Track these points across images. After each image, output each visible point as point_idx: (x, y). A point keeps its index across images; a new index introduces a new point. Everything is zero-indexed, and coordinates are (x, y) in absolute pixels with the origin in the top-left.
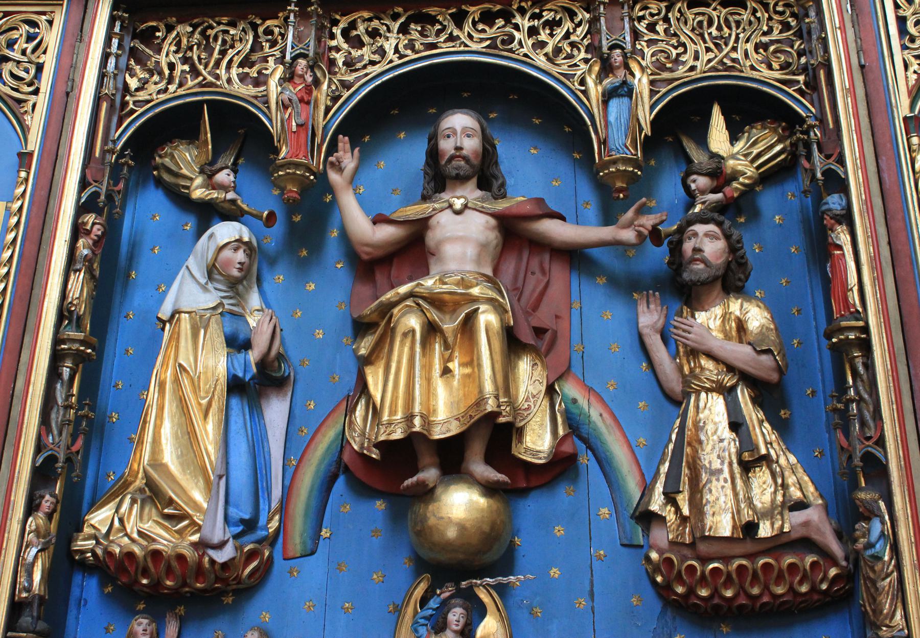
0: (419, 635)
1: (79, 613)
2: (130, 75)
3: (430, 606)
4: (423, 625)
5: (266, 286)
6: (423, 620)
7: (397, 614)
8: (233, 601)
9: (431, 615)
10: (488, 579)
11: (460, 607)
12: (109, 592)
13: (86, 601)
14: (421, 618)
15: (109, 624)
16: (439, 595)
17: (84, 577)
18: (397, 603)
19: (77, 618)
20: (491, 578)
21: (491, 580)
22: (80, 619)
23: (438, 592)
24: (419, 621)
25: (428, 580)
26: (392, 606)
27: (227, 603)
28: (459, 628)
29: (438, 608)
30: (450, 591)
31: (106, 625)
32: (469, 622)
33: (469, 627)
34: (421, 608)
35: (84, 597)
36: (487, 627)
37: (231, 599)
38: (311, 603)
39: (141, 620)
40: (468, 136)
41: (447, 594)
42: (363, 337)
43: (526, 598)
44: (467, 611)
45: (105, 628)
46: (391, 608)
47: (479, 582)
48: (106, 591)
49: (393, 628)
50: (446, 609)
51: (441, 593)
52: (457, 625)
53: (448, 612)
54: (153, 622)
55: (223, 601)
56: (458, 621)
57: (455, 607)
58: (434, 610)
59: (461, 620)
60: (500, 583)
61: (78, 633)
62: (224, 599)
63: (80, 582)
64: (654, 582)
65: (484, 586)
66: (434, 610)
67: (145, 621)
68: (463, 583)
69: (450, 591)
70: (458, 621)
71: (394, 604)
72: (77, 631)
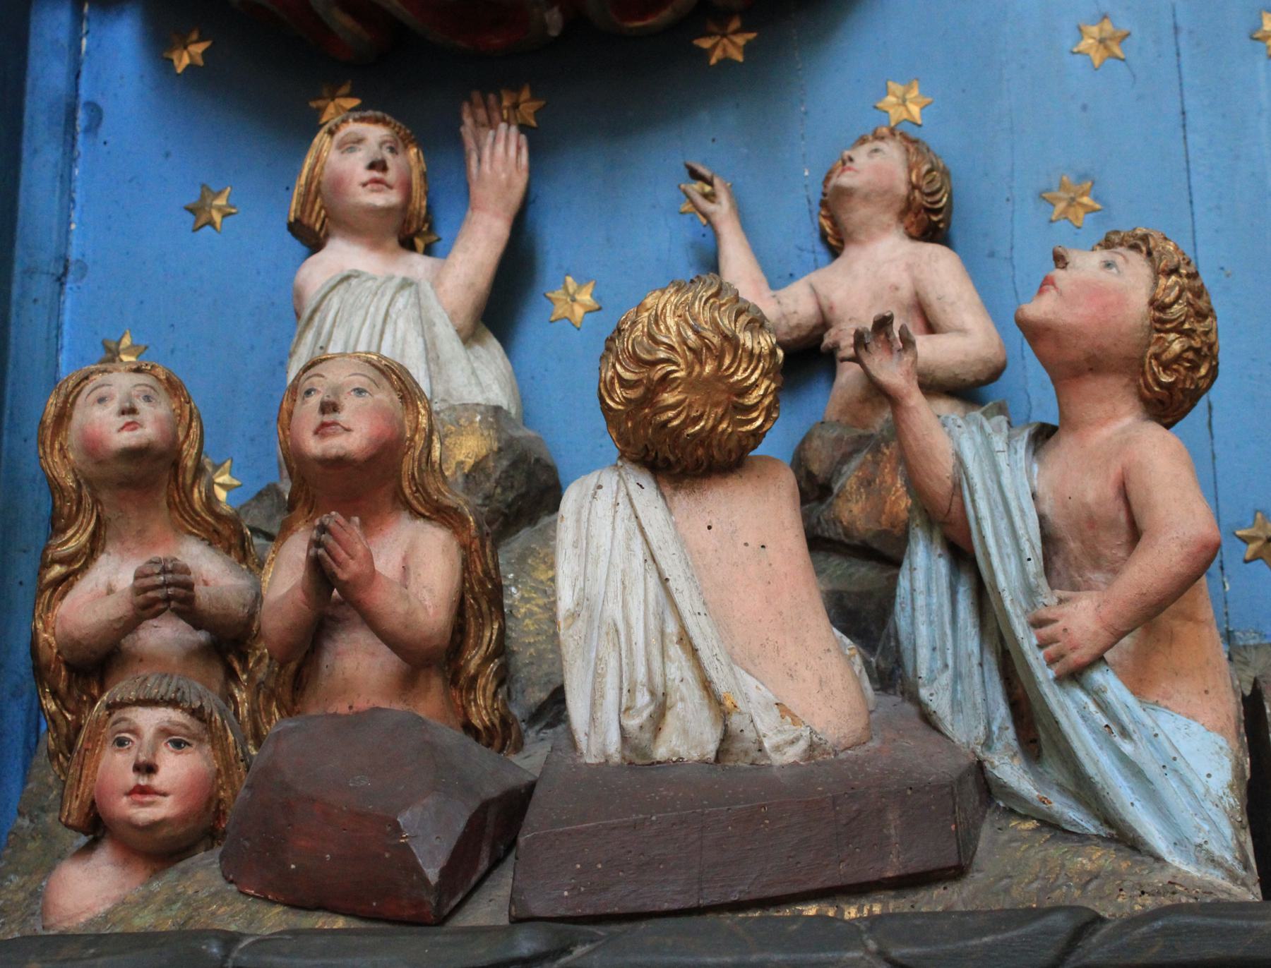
1: (70, 158)
2: (279, 494)
8: (748, 49)
12: (191, 68)
13: (96, 113)
15: (207, 193)
17: (78, 17)
19: (66, 179)
22: (78, 185)
27: (726, 62)
31: (192, 198)
35: (84, 94)
37: (741, 40)
38: (1108, 26)
39: (353, 128)
40: (178, 744)
45: (191, 210)
48: (182, 61)
54: (406, 142)
55: (706, 54)
61: (74, 240)
62: (705, 43)
63: (63, 36)
64: (606, 409)
67: (375, 134)
72: (68, 232)
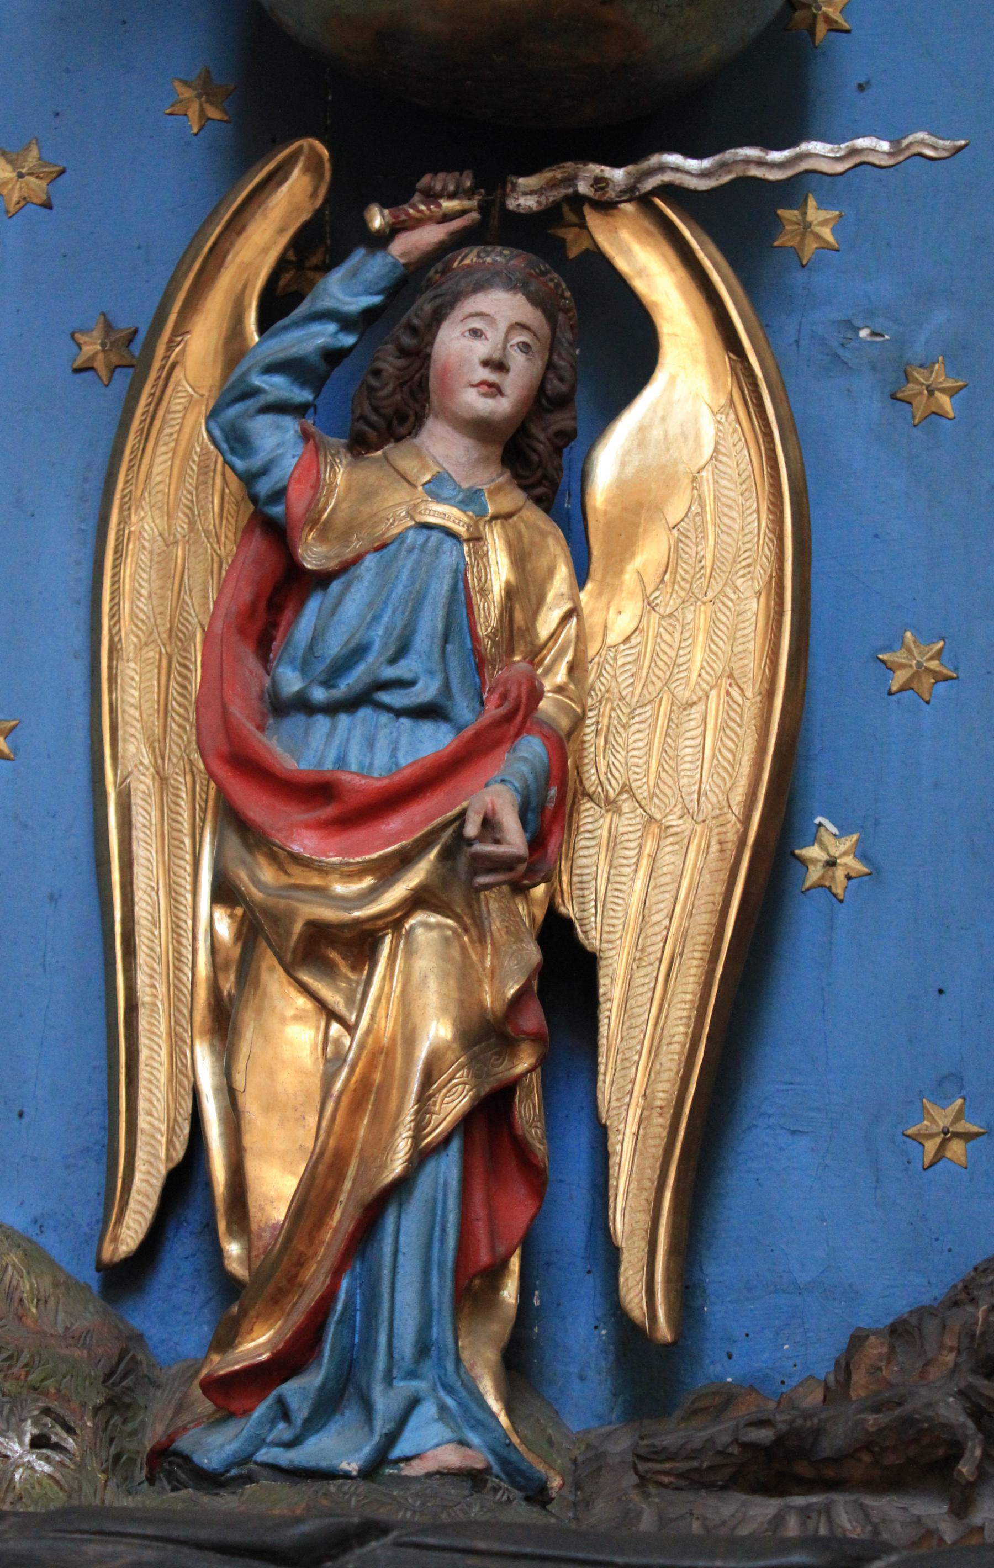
0: (256, 462)
3: (326, 303)
4: (280, 408)
5: (451, 1447)
6: (278, 380)
7: (122, 380)
9: (333, 356)
10: (674, 159)
11: (512, 285)
14: (271, 369)
16: (381, 241)
18: (124, 324)
20: (689, 154)
21: (693, 164)
23: (377, 220)
24: (257, 381)
25: (314, 167)
26: (97, 334)
28: (502, 406)
29: (370, 315)
30: (447, 218)
32: (556, 386)
33: (560, 421)
34: (264, 325)
36: (656, 433)
41: (431, 235)
42: (298, 692)
43: (870, 314)
44: (551, 318)
46: (92, 346)
47: (618, 175)
49: (100, 460)
50: (425, 305)
51: (394, 230)
52: (494, 390)
53: (438, 317)
56: (499, 366)
57: (479, 287)
58: (346, 322)
59: (518, 360)
60: (745, 182)
65: (645, 202)
66: (346, 322)
68: (505, 1293)
69: (447, 218)
70: (499, 366)
71: (108, 327)
